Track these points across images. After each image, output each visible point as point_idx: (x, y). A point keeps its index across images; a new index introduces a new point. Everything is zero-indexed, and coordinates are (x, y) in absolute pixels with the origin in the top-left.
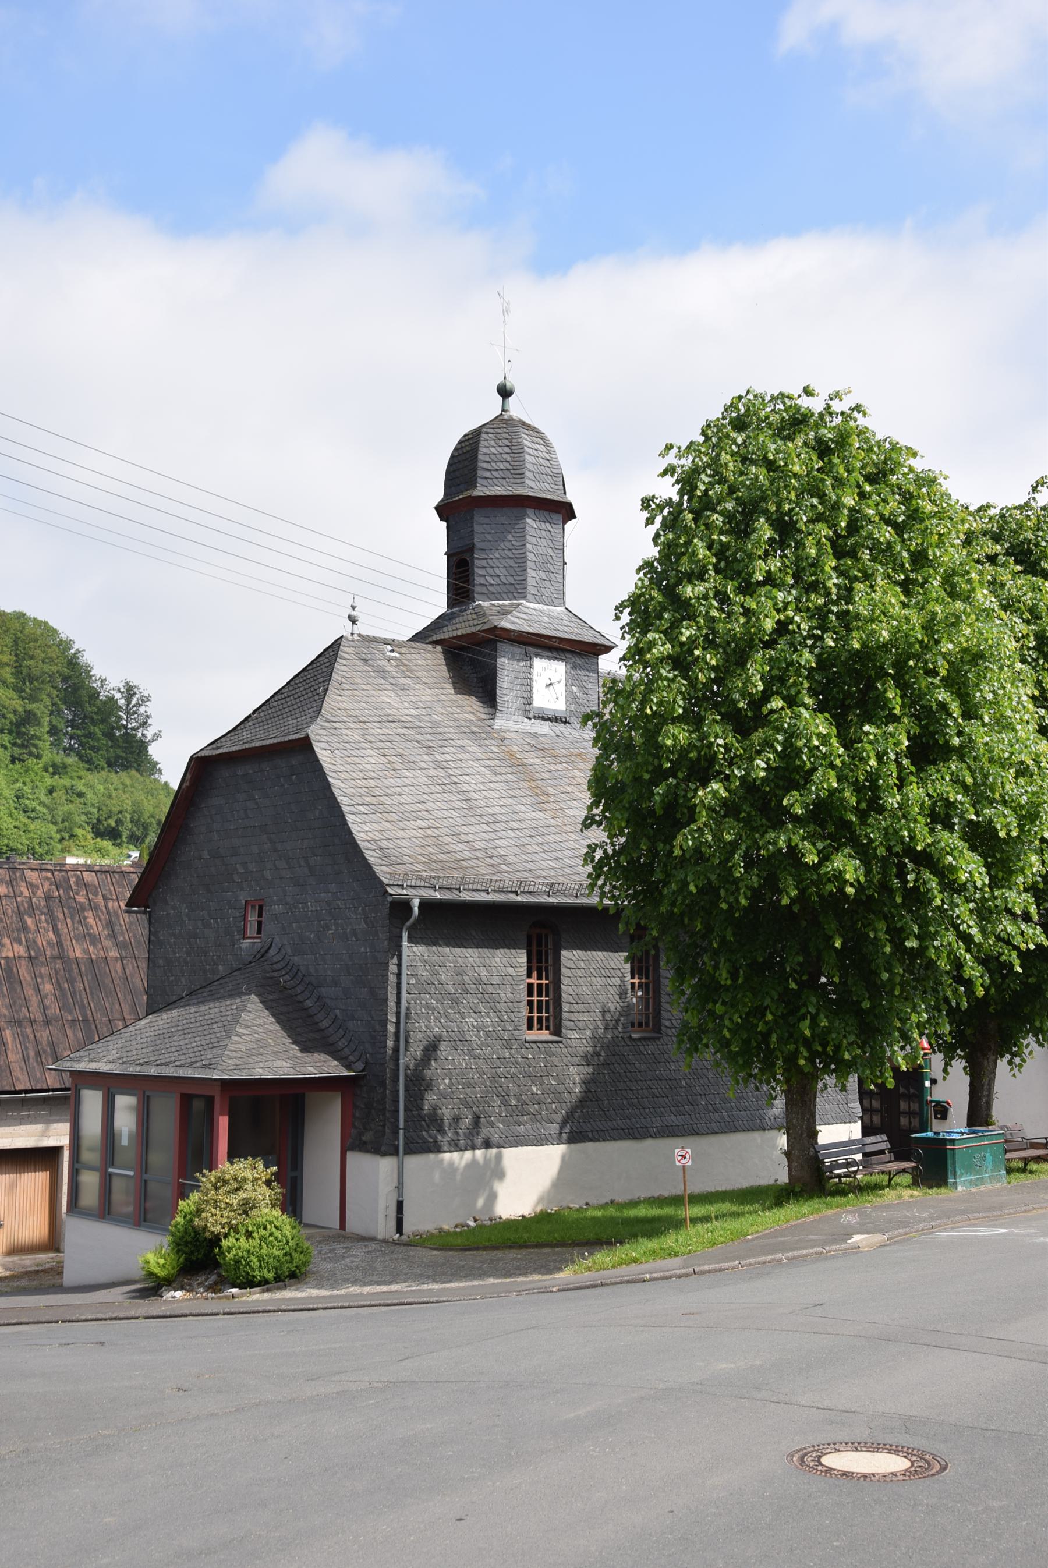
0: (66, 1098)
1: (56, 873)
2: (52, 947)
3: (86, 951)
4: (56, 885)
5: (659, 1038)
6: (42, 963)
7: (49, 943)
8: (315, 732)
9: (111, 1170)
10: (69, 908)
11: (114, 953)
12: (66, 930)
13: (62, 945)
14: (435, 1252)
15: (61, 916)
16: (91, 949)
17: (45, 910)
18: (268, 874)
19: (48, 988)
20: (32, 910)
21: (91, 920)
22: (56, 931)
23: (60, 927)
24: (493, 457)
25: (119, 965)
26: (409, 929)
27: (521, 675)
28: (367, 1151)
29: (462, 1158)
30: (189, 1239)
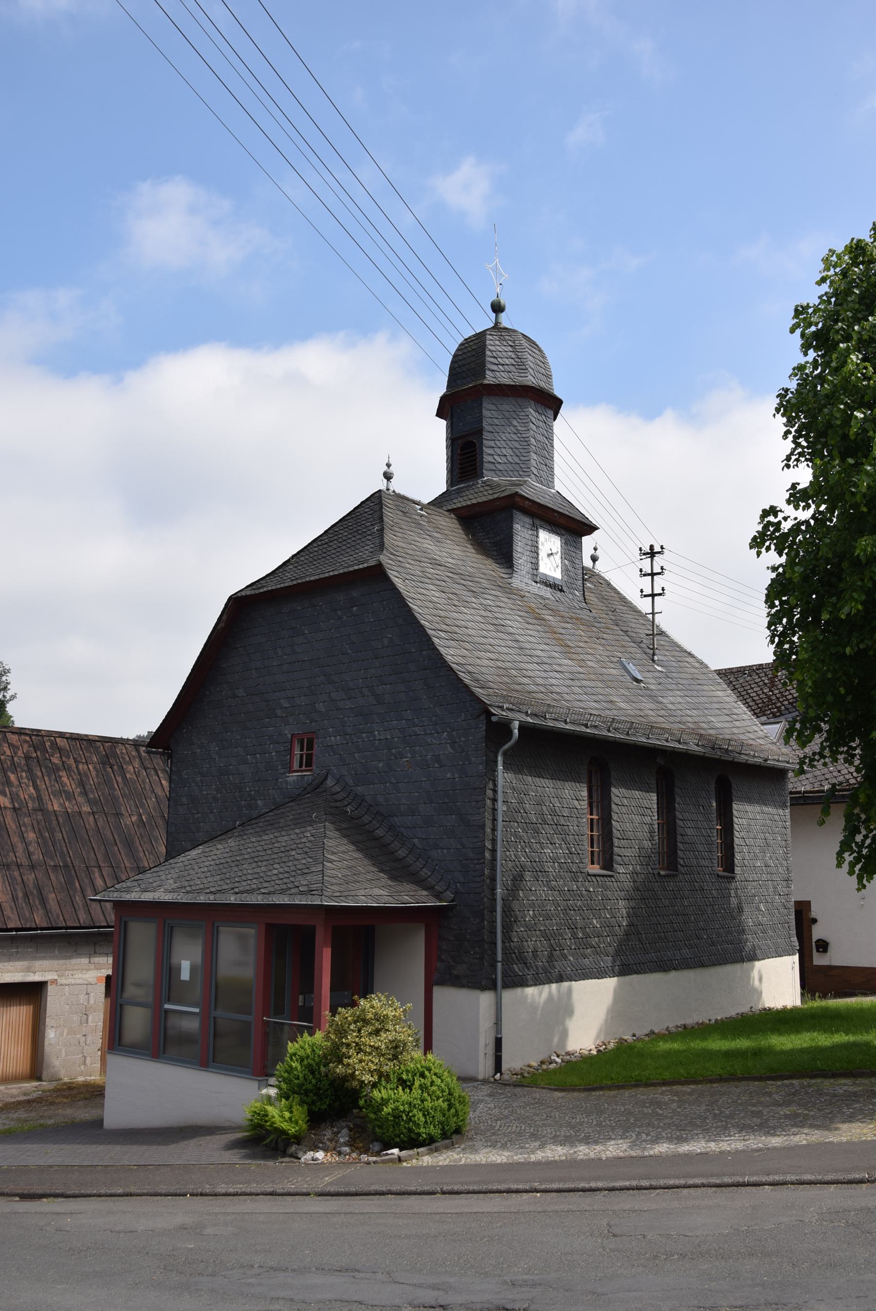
0: (111, 933)
1: (33, 737)
2: (33, 801)
3: (62, 805)
4: (34, 747)
5: (676, 876)
6: (25, 814)
7: (30, 797)
8: (385, 559)
9: (167, 1006)
10: (46, 767)
11: (86, 809)
12: (44, 786)
13: (42, 799)
14: (558, 1094)
15: (39, 774)
16: (67, 804)
17: (25, 768)
18: (321, 707)
19: (31, 836)
20: (14, 767)
21: (65, 779)
22: (36, 787)
23: (39, 783)
24: (499, 353)
25: (91, 819)
26: (505, 754)
27: (530, 543)
28: (462, 986)
29: (540, 994)
30: (310, 1087)
